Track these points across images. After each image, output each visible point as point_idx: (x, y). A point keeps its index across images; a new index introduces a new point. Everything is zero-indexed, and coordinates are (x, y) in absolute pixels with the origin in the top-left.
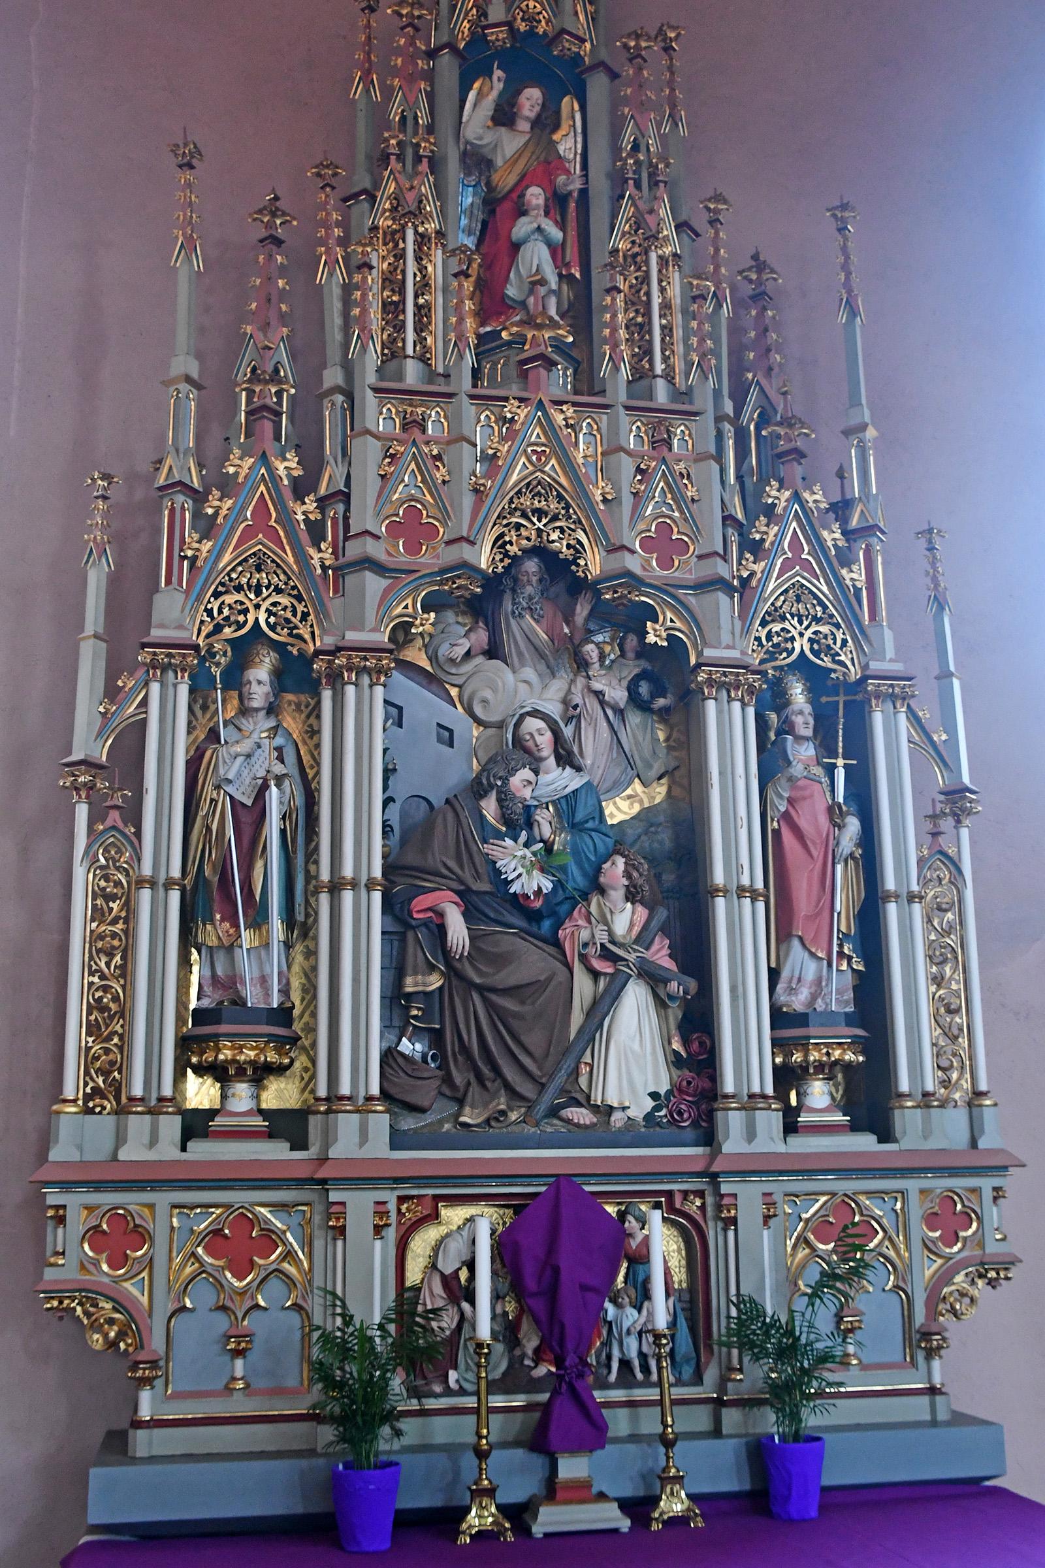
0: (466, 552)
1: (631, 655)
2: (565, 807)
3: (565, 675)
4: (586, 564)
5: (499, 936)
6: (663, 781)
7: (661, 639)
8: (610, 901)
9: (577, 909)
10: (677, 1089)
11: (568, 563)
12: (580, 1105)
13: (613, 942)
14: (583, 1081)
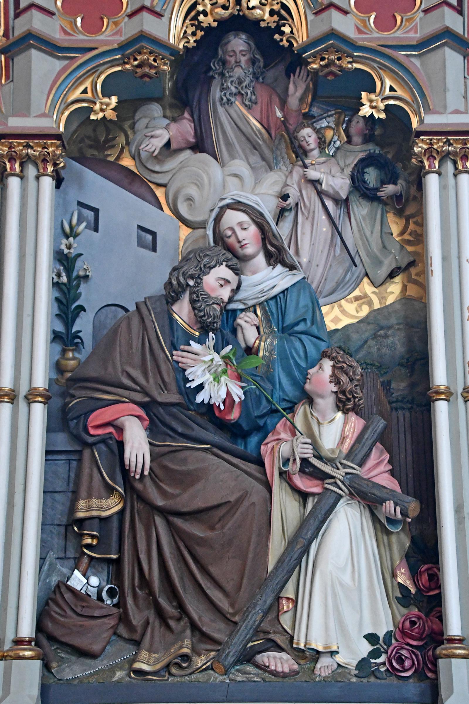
0: (149, 24)
1: (357, 139)
2: (274, 310)
3: (284, 168)
4: (292, 32)
5: (187, 453)
6: (398, 279)
7: (379, 111)
8: (318, 411)
9: (281, 422)
10: (402, 632)
11: (270, 31)
12: (281, 649)
13: (320, 458)
14: (286, 620)
